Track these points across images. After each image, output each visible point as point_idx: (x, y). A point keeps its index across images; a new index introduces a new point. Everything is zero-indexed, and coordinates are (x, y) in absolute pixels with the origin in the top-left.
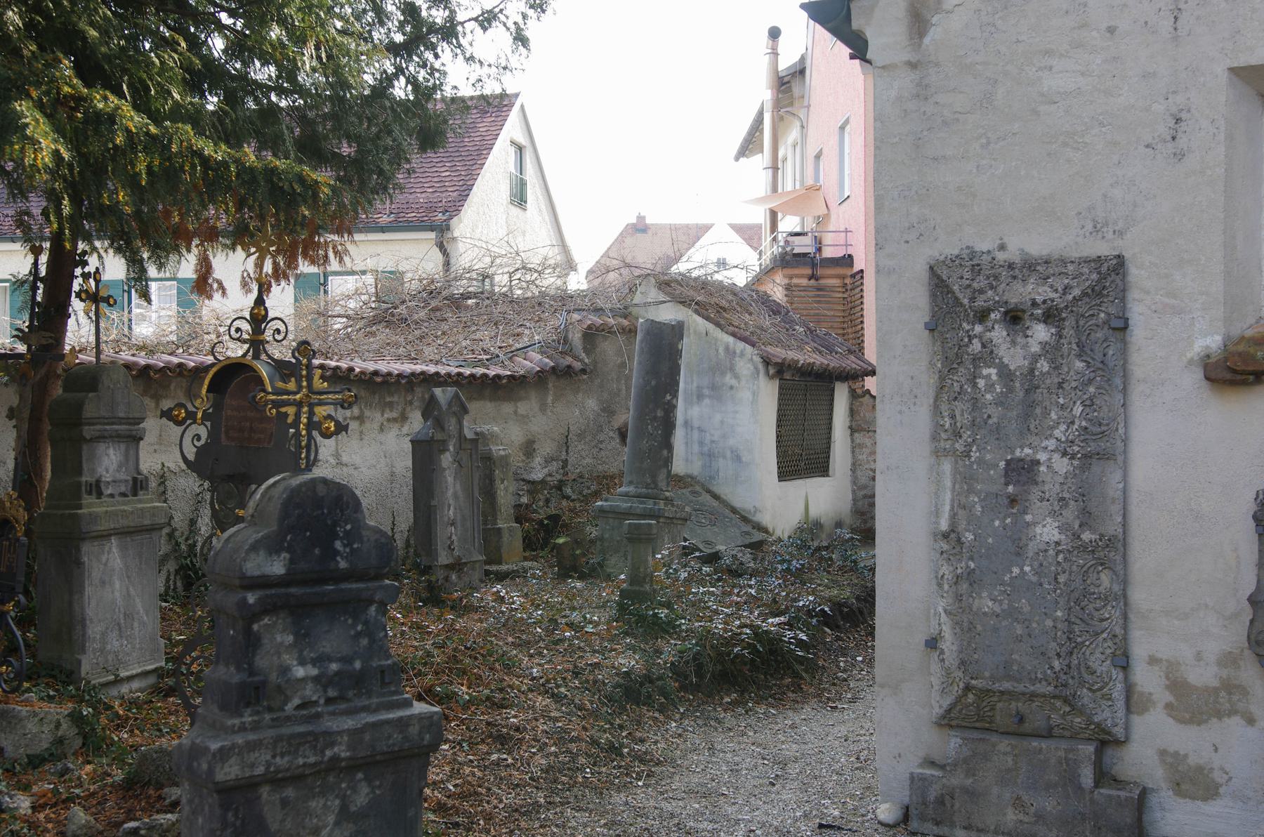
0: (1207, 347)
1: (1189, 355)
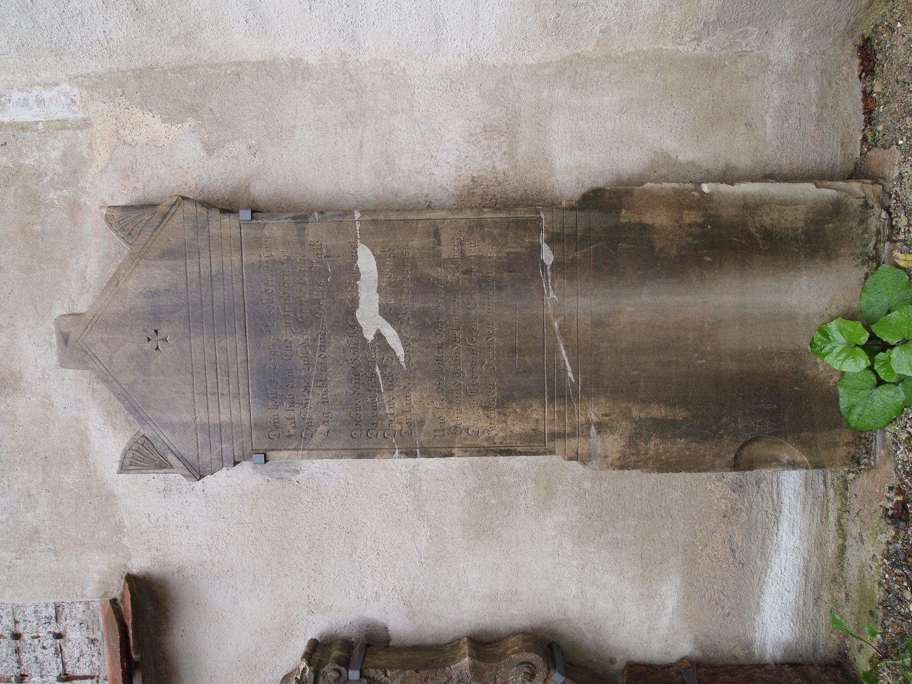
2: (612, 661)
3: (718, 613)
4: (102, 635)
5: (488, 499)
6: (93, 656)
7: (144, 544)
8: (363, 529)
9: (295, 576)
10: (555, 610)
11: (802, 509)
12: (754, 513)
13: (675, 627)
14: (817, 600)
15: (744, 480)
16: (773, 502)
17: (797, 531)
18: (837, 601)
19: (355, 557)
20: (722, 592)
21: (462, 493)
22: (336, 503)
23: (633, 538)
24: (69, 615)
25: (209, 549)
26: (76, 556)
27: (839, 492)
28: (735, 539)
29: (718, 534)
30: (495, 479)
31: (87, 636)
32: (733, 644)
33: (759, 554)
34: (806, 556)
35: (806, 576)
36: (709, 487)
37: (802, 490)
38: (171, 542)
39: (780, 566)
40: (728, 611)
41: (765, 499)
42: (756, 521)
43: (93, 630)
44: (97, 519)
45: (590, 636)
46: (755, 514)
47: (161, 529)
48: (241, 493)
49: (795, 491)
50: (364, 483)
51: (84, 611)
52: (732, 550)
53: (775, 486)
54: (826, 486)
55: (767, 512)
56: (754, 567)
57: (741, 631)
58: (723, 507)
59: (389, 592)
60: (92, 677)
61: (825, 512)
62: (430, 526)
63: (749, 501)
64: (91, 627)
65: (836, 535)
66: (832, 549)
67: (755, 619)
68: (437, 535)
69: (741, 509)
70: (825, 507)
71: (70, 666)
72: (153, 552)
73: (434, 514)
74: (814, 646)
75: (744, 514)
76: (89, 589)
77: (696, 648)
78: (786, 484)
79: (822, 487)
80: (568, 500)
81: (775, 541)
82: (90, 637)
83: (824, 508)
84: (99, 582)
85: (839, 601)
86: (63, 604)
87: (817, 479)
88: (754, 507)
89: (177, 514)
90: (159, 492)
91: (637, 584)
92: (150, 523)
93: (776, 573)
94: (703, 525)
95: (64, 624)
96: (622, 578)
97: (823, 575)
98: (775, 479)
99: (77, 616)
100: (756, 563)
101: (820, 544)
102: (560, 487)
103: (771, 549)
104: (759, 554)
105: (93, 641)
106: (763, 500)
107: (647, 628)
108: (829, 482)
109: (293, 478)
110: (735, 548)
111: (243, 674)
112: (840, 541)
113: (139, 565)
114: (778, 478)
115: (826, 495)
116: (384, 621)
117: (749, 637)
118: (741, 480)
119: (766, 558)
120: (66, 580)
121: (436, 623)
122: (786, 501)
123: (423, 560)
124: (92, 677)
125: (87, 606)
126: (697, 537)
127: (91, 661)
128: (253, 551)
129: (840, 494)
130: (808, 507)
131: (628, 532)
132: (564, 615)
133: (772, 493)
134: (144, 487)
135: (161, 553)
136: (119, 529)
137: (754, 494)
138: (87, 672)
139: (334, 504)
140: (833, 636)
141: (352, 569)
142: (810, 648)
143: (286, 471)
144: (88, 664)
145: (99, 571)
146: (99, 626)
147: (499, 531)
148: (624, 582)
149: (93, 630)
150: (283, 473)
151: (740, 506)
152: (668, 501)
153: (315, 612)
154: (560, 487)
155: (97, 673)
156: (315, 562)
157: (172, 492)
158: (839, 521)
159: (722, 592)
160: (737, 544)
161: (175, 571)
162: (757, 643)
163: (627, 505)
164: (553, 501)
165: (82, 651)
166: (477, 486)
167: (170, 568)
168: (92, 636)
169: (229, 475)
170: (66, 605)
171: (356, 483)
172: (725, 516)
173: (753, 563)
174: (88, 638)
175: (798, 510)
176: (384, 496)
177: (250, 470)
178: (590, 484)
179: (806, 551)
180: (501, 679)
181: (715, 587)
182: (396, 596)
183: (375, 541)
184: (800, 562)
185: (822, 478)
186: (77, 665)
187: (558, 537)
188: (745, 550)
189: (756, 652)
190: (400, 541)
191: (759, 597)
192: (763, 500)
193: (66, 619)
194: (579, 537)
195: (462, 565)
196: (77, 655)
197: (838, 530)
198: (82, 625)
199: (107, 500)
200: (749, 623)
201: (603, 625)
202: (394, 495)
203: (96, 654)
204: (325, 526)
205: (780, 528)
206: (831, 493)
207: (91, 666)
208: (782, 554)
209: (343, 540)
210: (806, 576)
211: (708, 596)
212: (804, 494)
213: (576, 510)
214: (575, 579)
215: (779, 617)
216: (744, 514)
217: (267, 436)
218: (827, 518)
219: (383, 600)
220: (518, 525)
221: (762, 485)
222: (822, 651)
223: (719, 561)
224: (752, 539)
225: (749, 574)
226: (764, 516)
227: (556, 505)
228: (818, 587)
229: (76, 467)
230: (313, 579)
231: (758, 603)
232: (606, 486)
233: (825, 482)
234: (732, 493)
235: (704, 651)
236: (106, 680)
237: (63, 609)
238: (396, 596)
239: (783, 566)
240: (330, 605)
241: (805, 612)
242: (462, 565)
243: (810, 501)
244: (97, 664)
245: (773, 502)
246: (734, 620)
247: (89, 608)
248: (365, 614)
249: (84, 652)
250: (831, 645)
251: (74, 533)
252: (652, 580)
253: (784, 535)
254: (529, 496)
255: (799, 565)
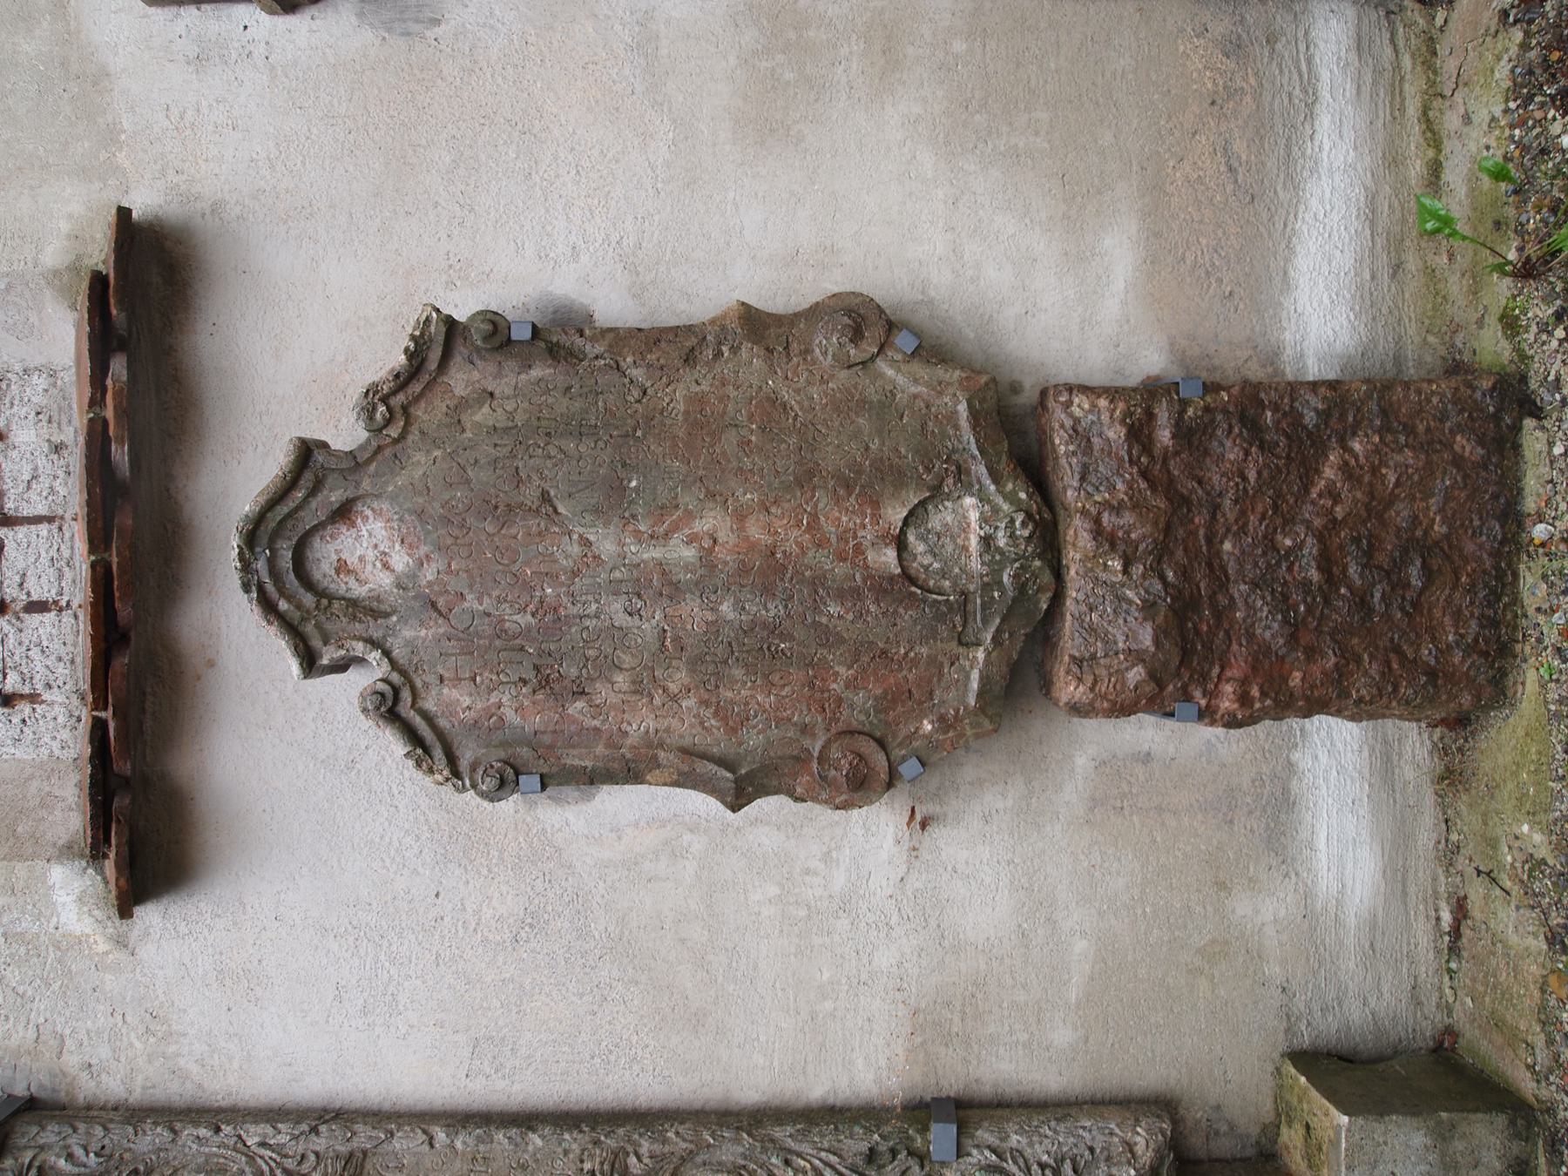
0: (80, 900)
1: (102, 946)
2: (1015, 388)
3: (1211, 291)
4: (76, 432)
5: (779, 71)
6: (55, 477)
7: (155, 162)
8: (551, 126)
9: (426, 215)
10: (905, 284)
11: (1354, 92)
12: (1267, 97)
13: (1132, 321)
14: (1397, 269)
15: (1244, 36)
16: (1301, 76)
17: (1349, 135)
18: (1433, 271)
19: (536, 178)
20: (1216, 251)
21: (733, 61)
22: (504, 78)
23: (1046, 145)
24: (18, 397)
25: (272, 167)
26: (32, 188)
27: (1421, 59)
28: (1235, 147)
29: (1204, 138)
30: (792, 35)
31: (47, 437)
32: (1242, 354)
33: (1282, 176)
34: (1369, 182)
35: (1372, 222)
36: (1182, 48)
37: (1353, 56)
38: (204, 157)
39: (1322, 201)
40: (1229, 289)
41: (1286, 71)
42: (1272, 111)
43: (59, 424)
44: (74, 118)
45: (972, 335)
46: (1269, 99)
47: (188, 132)
48: (333, 62)
49: (1339, 58)
50: (555, 43)
51: (46, 391)
52: (1230, 169)
53: (1302, 47)
54: (1396, 51)
55: (1290, 95)
56: (1272, 201)
57: (1257, 329)
58: (1209, 86)
59: (597, 245)
60: (50, 519)
61: (1398, 99)
62: (674, 121)
63: (1256, 74)
64: (55, 418)
65: (1422, 140)
66: (1416, 169)
67: (1281, 304)
68: (687, 138)
69: (1242, 89)
70: (1397, 91)
71: (12, 498)
72: (171, 176)
73: (681, 99)
74: (1398, 360)
75: (1248, 98)
76: (49, 250)
77: (1172, 362)
78: (1322, 45)
79: (1389, 51)
80: (925, 76)
81: (1309, 151)
82: (52, 439)
83: (1396, 91)
84: (68, 237)
85: (1437, 272)
86: (9, 375)
87: (1378, 39)
88: (1266, 85)
89: (218, 102)
90: (188, 63)
91: (1057, 234)
92: (167, 123)
93: (1315, 214)
94: (1174, 119)
95: (8, 413)
96: (1027, 221)
97: (1404, 221)
98: (1301, 34)
99: (33, 399)
100: (1275, 192)
101: (1393, 161)
102: (910, 50)
103: (1303, 167)
104: (1282, 176)
105: (58, 448)
106: (1281, 71)
107: (1078, 320)
108: (1401, 43)
109: (428, 33)
110: (1236, 165)
111: (320, 408)
112: (1431, 153)
113: (144, 202)
114: (1306, 33)
115: (1397, 67)
116: (586, 301)
117: (1272, 340)
118: (1239, 37)
119: (1293, 183)
120: (9, 235)
121: (683, 306)
122: (1325, 75)
123: (659, 185)
124: (50, 519)
125: (52, 380)
126: (1164, 143)
127: (51, 488)
128: (351, 169)
129: (1423, 63)
130: (1366, 89)
131: (1037, 133)
132: (923, 293)
133: (1298, 61)
134: (161, 54)
135: (185, 177)
136: (112, 136)
137: (1266, 60)
138: (41, 509)
139: (500, 80)
140: (1431, 339)
141: (531, 202)
142: (1389, 366)
143: (417, 21)
144: (44, 494)
145: (70, 216)
146: (71, 416)
147: (799, 132)
148: (1033, 229)
149: (59, 424)
150: (410, 24)
151: (1239, 83)
152: (1108, 74)
153: (458, 284)
154: (910, 50)
155: (60, 512)
156: (463, 187)
157: (212, 62)
158: (1425, 113)
159: (1216, 251)
160: (1239, 157)
161: (208, 212)
162: (1289, 351)
163: (1033, 83)
164: (898, 76)
165: (36, 469)
166: (760, 47)
167: (199, 205)
168: (56, 439)
169: (315, 28)
170: (14, 378)
171: (541, 43)
172: (1213, 103)
173: (1272, 194)
174: (49, 441)
175: (1348, 94)
176: (590, 66)
177: (353, 19)
178: (964, 46)
179: (1369, 175)
180: (799, 343)
181: (1204, 241)
182: (610, 253)
183: (572, 149)
184: (1358, 194)
185: (1388, 36)
186: (25, 496)
187: (908, 142)
188: (1254, 167)
189: (1288, 370)
190: (619, 149)
191: (1287, 260)
192: (1281, 71)
193: (12, 404)
194: (947, 143)
195: (732, 195)
196: (27, 477)
197: (1424, 133)
198: (40, 417)
199: (95, 84)
200: (1271, 311)
201: (995, 315)
202: (608, 64)
203: (60, 473)
204: (482, 121)
205: (1317, 127)
206: (1407, 62)
207: (50, 498)
208: (1324, 178)
209: (514, 146)
210: (1372, 224)
211: (1189, 260)
212: (1357, 64)
213: (940, 93)
214: (941, 225)
215: (1326, 301)
216: (1248, 98)
217: (414, 429)
218: (1402, 109)
219: (584, 259)
220: (834, 118)
221: (1279, 46)
222: (1412, 371)
223: (1208, 189)
224: (1266, 145)
225: (1264, 216)
226: (1286, 101)
227: (904, 83)
228: (1396, 245)
229: (45, 24)
230: (457, 221)
231: (1285, 273)
232: (994, 47)
233: (1392, 41)
234: (1224, 59)
235: (1187, 368)
236: (75, 520)
237: (8, 386)
238: (610, 253)
239: (1327, 201)
240: (487, 269)
241: (1375, 293)
242: (732, 195)
243: (1368, 78)
244: (62, 493)
245: (1301, 76)
246: (1241, 306)
247: (55, 385)
248: (550, 289)
249: (41, 470)
250: (1429, 359)
251: (31, 146)
252: (1085, 226)
253: (1325, 140)
254: (854, 66)
255: (1358, 200)
